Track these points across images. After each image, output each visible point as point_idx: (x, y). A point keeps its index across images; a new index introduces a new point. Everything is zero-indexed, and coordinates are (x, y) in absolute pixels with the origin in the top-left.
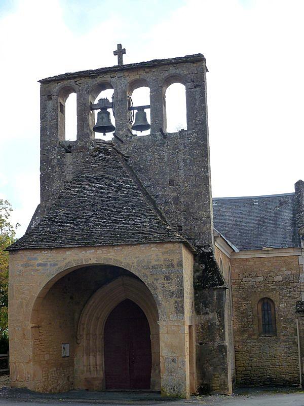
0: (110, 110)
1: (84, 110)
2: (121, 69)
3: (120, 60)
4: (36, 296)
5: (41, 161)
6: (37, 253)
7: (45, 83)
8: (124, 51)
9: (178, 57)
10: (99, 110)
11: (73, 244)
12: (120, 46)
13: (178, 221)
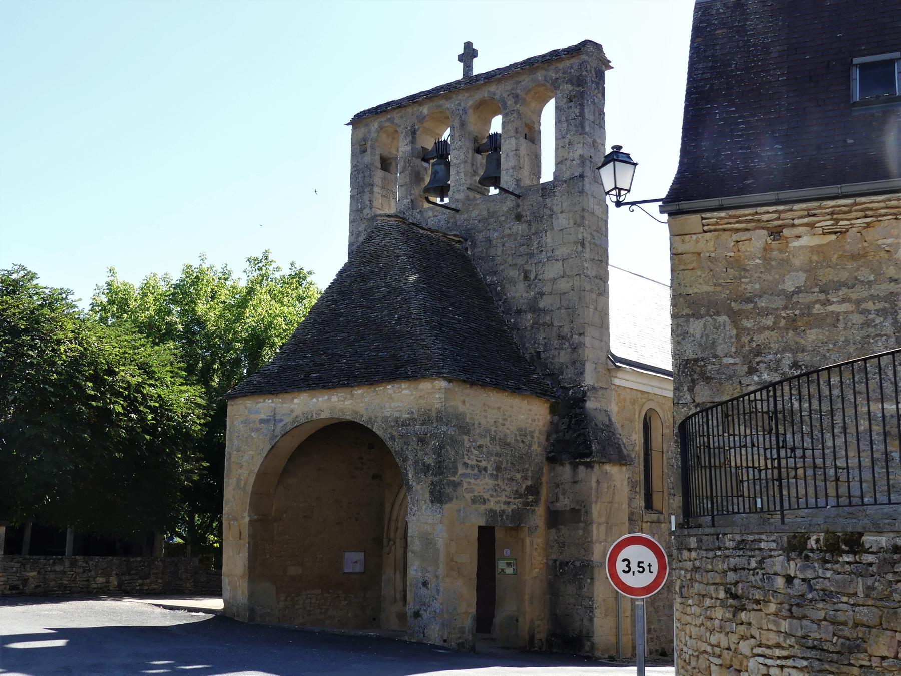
3: (468, 67)
4: (256, 471)
12: (468, 45)
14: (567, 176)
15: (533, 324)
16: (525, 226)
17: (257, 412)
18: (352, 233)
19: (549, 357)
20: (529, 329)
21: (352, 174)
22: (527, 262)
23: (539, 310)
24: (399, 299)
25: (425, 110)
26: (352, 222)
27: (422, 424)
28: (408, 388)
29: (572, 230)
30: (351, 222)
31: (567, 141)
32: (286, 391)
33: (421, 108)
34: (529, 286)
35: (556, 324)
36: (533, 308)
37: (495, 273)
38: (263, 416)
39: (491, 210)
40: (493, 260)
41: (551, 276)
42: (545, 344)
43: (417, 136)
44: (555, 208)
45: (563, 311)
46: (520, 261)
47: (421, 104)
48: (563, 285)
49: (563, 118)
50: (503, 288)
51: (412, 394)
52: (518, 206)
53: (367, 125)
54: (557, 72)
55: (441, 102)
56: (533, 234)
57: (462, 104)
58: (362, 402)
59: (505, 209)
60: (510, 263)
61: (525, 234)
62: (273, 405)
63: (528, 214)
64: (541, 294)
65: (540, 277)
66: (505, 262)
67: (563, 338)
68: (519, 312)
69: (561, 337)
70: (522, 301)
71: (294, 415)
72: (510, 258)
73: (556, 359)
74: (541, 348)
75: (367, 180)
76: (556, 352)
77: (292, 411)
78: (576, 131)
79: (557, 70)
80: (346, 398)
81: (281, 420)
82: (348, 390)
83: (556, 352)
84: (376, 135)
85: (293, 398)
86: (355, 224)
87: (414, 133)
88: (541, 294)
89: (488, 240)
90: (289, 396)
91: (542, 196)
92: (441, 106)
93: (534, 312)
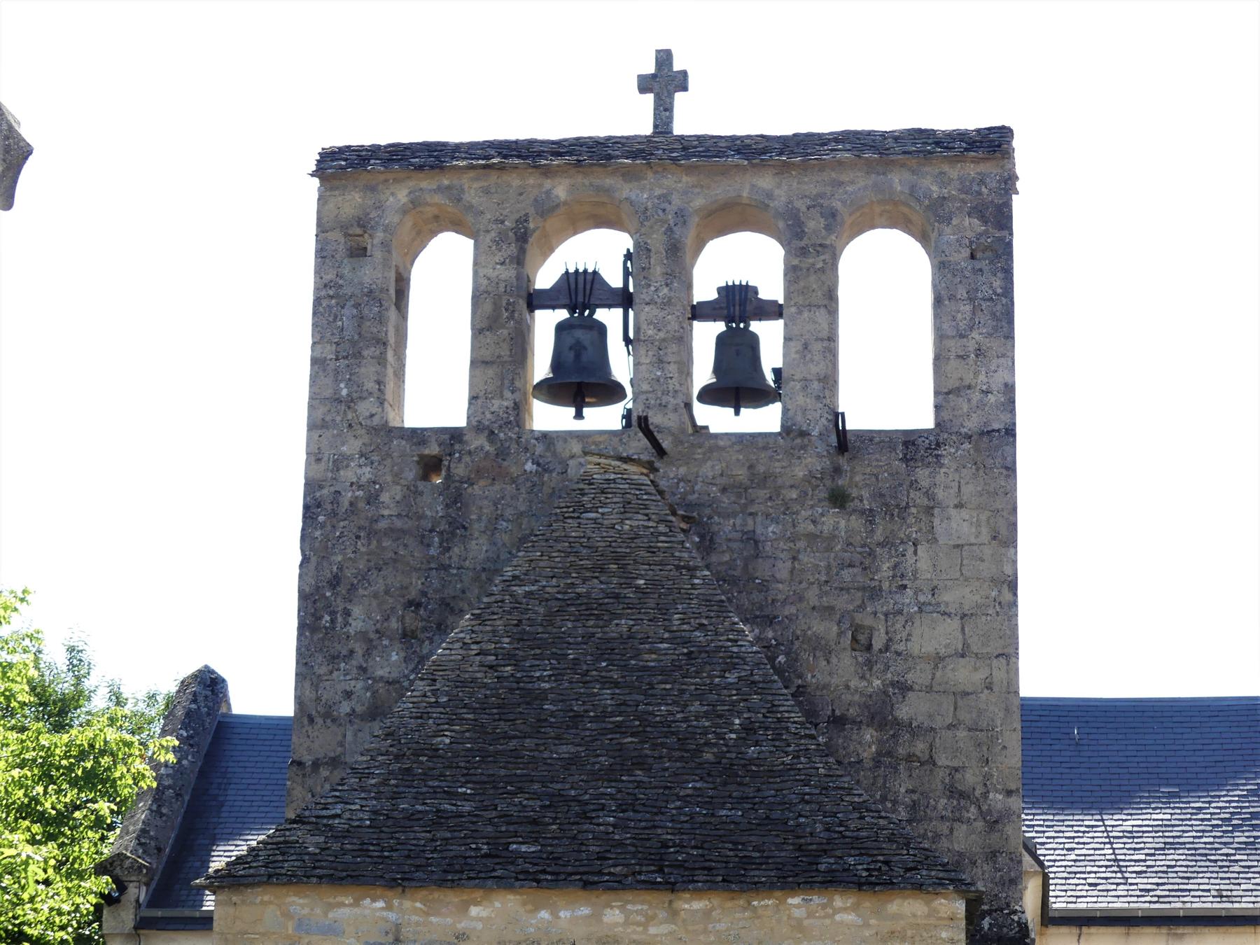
0: (610, 318)
1: (500, 314)
2: (662, 151)
3: (664, 111)
5: (306, 508)
6: (343, 905)
7: (340, 167)
8: (681, 82)
9: (296, 571)
10: (563, 314)
11: (382, 882)
12: (664, 58)
14: (972, 424)
15: (879, 753)
16: (856, 522)
18: (314, 456)
20: (868, 764)
21: (317, 302)
22: (862, 607)
23: (897, 723)
24: (732, 678)
25: (561, 190)
26: (315, 426)
28: (855, 908)
29: (987, 551)
30: (312, 427)
31: (972, 346)
32: (442, 883)
33: (548, 184)
34: (869, 664)
35: (942, 760)
36: (879, 714)
40: (764, 587)
41: (929, 648)
42: (914, 806)
43: (528, 247)
44: (940, 494)
45: (962, 734)
46: (842, 602)
47: (547, 172)
48: (964, 674)
49: (962, 292)
50: (793, 659)
51: (867, 925)
52: (837, 470)
53: (373, 189)
54: (943, 185)
55: (608, 181)
57: (677, 201)
58: (705, 931)
59: (800, 472)
60: (814, 601)
61: (857, 539)
62: (392, 916)
63: (865, 494)
65: (901, 647)
66: (801, 599)
67: (962, 795)
68: (838, 722)
69: (956, 793)
70: (847, 697)
72: (815, 590)
73: (944, 844)
75: (370, 327)
76: (944, 828)
78: (995, 329)
79: (942, 179)
80: (650, 919)
82: (666, 897)
83: (944, 828)
84: (396, 219)
85: (465, 907)
87: (522, 238)
89: (751, 539)
90: (452, 897)
91: (905, 459)
92: (608, 191)
93: (881, 727)
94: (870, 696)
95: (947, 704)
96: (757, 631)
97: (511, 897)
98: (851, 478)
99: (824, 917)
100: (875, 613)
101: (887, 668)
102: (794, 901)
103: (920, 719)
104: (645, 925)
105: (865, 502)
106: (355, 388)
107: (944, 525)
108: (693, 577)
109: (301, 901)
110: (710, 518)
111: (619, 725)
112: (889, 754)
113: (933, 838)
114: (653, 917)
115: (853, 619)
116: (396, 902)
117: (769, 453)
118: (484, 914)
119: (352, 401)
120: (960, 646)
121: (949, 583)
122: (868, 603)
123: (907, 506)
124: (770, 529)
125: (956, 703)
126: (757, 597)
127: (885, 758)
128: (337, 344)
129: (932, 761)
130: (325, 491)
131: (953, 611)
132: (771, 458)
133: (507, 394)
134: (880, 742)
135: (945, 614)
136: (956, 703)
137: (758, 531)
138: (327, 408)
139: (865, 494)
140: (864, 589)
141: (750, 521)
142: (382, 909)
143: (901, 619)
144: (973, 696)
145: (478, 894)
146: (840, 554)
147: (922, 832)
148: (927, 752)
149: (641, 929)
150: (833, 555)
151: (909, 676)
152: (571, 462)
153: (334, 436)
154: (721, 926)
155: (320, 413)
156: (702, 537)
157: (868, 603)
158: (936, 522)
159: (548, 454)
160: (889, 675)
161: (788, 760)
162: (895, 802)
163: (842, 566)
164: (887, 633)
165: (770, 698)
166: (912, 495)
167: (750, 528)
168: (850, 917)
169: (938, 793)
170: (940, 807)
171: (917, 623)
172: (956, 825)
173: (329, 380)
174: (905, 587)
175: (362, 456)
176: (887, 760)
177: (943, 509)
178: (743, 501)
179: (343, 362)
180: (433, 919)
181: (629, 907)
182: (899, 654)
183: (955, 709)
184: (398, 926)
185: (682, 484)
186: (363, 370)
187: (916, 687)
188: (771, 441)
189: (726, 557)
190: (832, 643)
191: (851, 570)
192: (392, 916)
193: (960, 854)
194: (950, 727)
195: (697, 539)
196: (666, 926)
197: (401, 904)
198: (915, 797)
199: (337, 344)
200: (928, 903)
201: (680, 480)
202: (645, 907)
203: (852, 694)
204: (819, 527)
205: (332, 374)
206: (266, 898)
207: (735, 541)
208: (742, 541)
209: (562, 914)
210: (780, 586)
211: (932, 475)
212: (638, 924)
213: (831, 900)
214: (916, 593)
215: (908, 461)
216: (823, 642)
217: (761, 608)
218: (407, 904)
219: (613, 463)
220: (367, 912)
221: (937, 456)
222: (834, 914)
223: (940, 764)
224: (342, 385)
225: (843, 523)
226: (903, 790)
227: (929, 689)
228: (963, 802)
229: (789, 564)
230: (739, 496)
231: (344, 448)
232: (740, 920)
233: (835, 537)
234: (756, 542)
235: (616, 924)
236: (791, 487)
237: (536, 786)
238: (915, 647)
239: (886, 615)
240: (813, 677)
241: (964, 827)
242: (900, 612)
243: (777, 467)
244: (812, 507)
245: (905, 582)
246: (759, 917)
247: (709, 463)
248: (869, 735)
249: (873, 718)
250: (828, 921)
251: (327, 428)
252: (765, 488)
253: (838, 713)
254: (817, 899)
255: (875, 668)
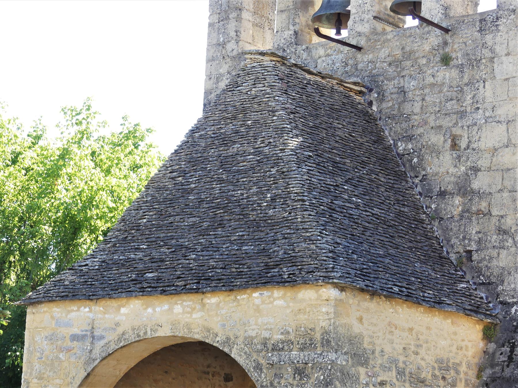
6: (73, 311)
13: (464, 238)
15: (463, 211)
17: (68, 325)
19: (484, 259)
20: (457, 218)
22: (456, 124)
23: (473, 192)
24: (274, 171)
27: (301, 350)
28: (283, 297)
34: (459, 157)
35: (495, 212)
36: (464, 189)
37: (410, 138)
38: (76, 331)
39: (408, 49)
40: (408, 119)
41: (490, 145)
42: (479, 242)
44: (498, 49)
45: (506, 194)
46: (446, 122)
50: (421, 159)
51: (288, 307)
56: (467, 85)
59: (427, 48)
60: (432, 124)
62: (91, 315)
63: (459, 55)
64: (476, 170)
65: (475, 146)
66: (426, 123)
67: (505, 232)
68: (442, 194)
69: (502, 231)
70: (447, 179)
71: (120, 330)
72: (433, 117)
73: (495, 263)
74: (473, 247)
77: (117, 324)
81: (102, 337)
82: (199, 296)
83: (494, 253)
85: (120, 307)
86: (214, 63)
88: (476, 170)
89: (402, 91)
90: (113, 303)
91: (481, 30)
93: (464, 195)
94: (459, 177)
95: (498, 176)
96: (404, 145)
97: (137, 302)
98: (452, 46)
99: (269, 303)
100: (462, 127)
101: (468, 158)
102: (256, 295)
103: (484, 188)
104: (191, 313)
105: (459, 60)
106: (226, 36)
107: (499, 68)
108: (274, 116)
109: (58, 310)
110: (383, 82)
111: (218, 203)
112: (468, 211)
113: (489, 259)
114: (194, 309)
115: (451, 131)
116: (93, 308)
117: (412, 38)
118: (126, 312)
119: (225, 44)
120: (506, 141)
121: (502, 103)
122: (459, 121)
123: (481, 59)
124: (412, 84)
125: (503, 176)
126: (404, 125)
127: (466, 213)
128: (219, 14)
129: (490, 213)
130: (213, 95)
131: (503, 120)
132: (412, 41)
133: (291, 27)
134: (464, 204)
135: (499, 122)
136: (503, 176)
137: (406, 86)
138: (214, 50)
139: (459, 55)
140: (457, 113)
141: (402, 80)
142: (88, 312)
143: (476, 128)
144: (512, 171)
145: (124, 301)
146: (446, 93)
147: (483, 256)
148: (487, 207)
149: (189, 315)
150: (442, 94)
151: (479, 163)
152: (319, 61)
153: (217, 64)
154: (223, 312)
155: (211, 54)
156: (379, 94)
157: (459, 121)
158: (495, 66)
159: (309, 58)
160: (469, 163)
161: (286, 215)
162: (470, 240)
163: (447, 101)
164: (468, 138)
165: (287, 180)
166: (483, 52)
167: (402, 85)
168: (280, 303)
169: (492, 232)
170: (493, 240)
171: (484, 129)
172: (501, 251)
173: (215, 35)
174: (478, 108)
175: (228, 73)
176: (467, 214)
177: (499, 57)
178: (399, 70)
179: (222, 23)
180: (106, 316)
181: (184, 303)
182: (474, 149)
183: (503, 179)
184: (93, 320)
185: (370, 64)
186: (230, 26)
187: (483, 169)
188: (413, 31)
189: (390, 104)
190: (440, 148)
191: (451, 102)
192: (91, 315)
193: (503, 268)
194: (500, 191)
195: (376, 95)
196: (199, 313)
197: (95, 309)
198: (480, 236)
199: (219, 14)
200: (317, 292)
201: (369, 62)
202: (191, 303)
203: (450, 177)
204: (436, 79)
205: (217, 31)
206: (45, 309)
207: (395, 93)
208: (398, 93)
209: (157, 310)
210: (416, 117)
211: (494, 38)
212: (188, 313)
213: (273, 293)
214: (484, 112)
215: (482, 31)
216: (436, 148)
217: (406, 132)
218: (97, 308)
219: (257, 57)
220: (82, 314)
221: (497, 25)
222: (274, 301)
223: (493, 214)
224: (221, 36)
225: (448, 75)
226: (474, 232)
227: (489, 169)
228: (505, 236)
229: (420, 103)
230: (397, 66)
231: (221, 70)
232: (232, 307)
233: (444, 83)
234: (405, 92)
235: (179, 314)
236: (423, 57)
237: (173, 241)
238: (482, 145)
239: (468, 127)
240: (431, 169)
241: (505, 251)
242: (475, 124)
243: (415, 46)
244: (433, 67)
245: (478, 106)
246: (240, 305)
247: (383, 50)
248: (457, 200)
249: (460, 190)
250: (270, 306)
251: (214, 61)
252: (410, 60)
253: (443, 189)
254: (266, 293)
255: (462, 160)
